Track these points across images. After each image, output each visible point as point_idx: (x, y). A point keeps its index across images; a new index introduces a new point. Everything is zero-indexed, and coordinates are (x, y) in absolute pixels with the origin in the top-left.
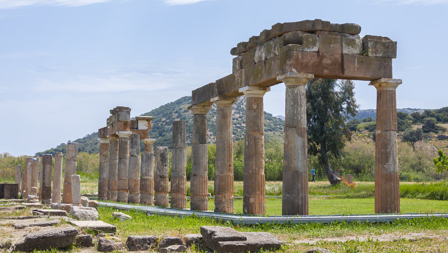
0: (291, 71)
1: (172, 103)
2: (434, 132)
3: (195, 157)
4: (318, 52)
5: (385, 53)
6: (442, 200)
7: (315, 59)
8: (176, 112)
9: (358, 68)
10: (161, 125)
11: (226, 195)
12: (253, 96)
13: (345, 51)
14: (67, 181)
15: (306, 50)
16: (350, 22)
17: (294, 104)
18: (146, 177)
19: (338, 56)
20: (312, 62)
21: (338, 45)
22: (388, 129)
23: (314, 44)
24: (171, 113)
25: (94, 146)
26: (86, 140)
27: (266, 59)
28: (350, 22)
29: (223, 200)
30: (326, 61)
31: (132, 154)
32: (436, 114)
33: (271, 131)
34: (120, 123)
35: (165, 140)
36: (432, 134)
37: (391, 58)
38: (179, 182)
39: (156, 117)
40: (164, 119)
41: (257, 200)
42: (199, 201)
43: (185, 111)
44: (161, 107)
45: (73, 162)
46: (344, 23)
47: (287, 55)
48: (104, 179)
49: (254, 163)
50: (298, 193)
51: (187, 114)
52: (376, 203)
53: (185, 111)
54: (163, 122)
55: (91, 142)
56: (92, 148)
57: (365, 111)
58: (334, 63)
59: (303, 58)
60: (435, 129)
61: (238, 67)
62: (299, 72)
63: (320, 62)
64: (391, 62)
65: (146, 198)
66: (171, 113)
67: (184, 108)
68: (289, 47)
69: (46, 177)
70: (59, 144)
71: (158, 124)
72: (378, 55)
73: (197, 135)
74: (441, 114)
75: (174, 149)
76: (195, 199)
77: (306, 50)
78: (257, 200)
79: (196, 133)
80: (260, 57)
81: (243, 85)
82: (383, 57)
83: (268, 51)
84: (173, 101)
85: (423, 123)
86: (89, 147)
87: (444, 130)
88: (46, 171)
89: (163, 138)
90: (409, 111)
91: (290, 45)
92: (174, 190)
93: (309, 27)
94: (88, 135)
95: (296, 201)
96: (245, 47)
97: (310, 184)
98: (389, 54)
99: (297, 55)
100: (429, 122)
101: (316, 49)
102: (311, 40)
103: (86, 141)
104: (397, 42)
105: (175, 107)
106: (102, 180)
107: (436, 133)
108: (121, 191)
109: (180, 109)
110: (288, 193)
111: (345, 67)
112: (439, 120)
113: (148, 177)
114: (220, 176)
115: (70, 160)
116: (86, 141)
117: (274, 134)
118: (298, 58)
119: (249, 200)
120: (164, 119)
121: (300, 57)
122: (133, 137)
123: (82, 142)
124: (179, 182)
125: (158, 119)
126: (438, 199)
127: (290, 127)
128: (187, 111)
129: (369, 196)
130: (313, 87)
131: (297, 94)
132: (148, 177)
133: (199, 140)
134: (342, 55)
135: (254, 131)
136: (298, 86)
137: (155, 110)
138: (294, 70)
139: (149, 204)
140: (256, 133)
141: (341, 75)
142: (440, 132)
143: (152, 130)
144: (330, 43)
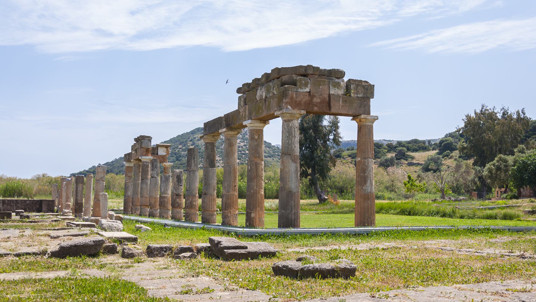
0: (287, 108)
2: (404, 159)
4: (310, 92)
5: (364, 94)
6: (410, 215)
7: (307, 98)
8: (191, 141)
9: (342, 106)
10: (178, 151)
12: (255, 128)
13: (332, 92)
16: (336, 68)
17: (289, 135)
19: (326, 96)
20: (304, 100)
21: (326, 87)
22: (366, 157)
23: (306, 85)
24: (186, 141)
26: (113, 163)
28: (336, 68)
29: (229, 215)
30: (316, 100)
32: (406, 145)
33: (270, 157)
35: (181, 164)
38: (192, 199)
39: (173, 144)
40: (180, 147)
41: (258, 215)
42: (209, 215)
43: (198, 140)
45: (102, 182)
47: (284, 95)
50: (292, 209)
54: (180, 148)
55: (118, 165)
57: (348, 141)
58: (322, 102)
59: (297, 97)
61: (242, 104)
62: (293, 108)
65: (164, 213)
66: (186, 141)
68: (285, 87)
72: (359, 96)
73: (208, 161)
74: (410, 145)
78: (258, 215)
79: (207, 158)
80: (261, 96)
82: (363, 98)
83: (268, 91)
85: (396, 152)
87: (413, 158)
88: (78, 189)
89: (180, 163)
90: (384, 142)
91: (286, 86)
93: (302, 71)
95: (290, 216)
98: (368, 95)
100: (400, 151)
101: (307, 90)
103: (114, 164)
105: (190, 136)
107: (407, 160)
108: (143, 207)
109: (195, 138)
110: (283, 210)
111: (332, 105)
112: (409, 149)
113: (166, 195)
115: (99, 180)
116: (114, 164)
119: (251, 215)
120: (180, 147)
121: (294, 96)
123: (111, 165)
124: (192, 199)
125: (176, 146)
126: (407, 215)
129: (350, 212)
131: (291, 127)
132: (166, 195)
133: (210, 165)
134: (329, 95)
135: (256, 157)
137: (173, 139)
139: (167, 218)
140: (257, 159)
141: (329, 112)
144: (319, 85)
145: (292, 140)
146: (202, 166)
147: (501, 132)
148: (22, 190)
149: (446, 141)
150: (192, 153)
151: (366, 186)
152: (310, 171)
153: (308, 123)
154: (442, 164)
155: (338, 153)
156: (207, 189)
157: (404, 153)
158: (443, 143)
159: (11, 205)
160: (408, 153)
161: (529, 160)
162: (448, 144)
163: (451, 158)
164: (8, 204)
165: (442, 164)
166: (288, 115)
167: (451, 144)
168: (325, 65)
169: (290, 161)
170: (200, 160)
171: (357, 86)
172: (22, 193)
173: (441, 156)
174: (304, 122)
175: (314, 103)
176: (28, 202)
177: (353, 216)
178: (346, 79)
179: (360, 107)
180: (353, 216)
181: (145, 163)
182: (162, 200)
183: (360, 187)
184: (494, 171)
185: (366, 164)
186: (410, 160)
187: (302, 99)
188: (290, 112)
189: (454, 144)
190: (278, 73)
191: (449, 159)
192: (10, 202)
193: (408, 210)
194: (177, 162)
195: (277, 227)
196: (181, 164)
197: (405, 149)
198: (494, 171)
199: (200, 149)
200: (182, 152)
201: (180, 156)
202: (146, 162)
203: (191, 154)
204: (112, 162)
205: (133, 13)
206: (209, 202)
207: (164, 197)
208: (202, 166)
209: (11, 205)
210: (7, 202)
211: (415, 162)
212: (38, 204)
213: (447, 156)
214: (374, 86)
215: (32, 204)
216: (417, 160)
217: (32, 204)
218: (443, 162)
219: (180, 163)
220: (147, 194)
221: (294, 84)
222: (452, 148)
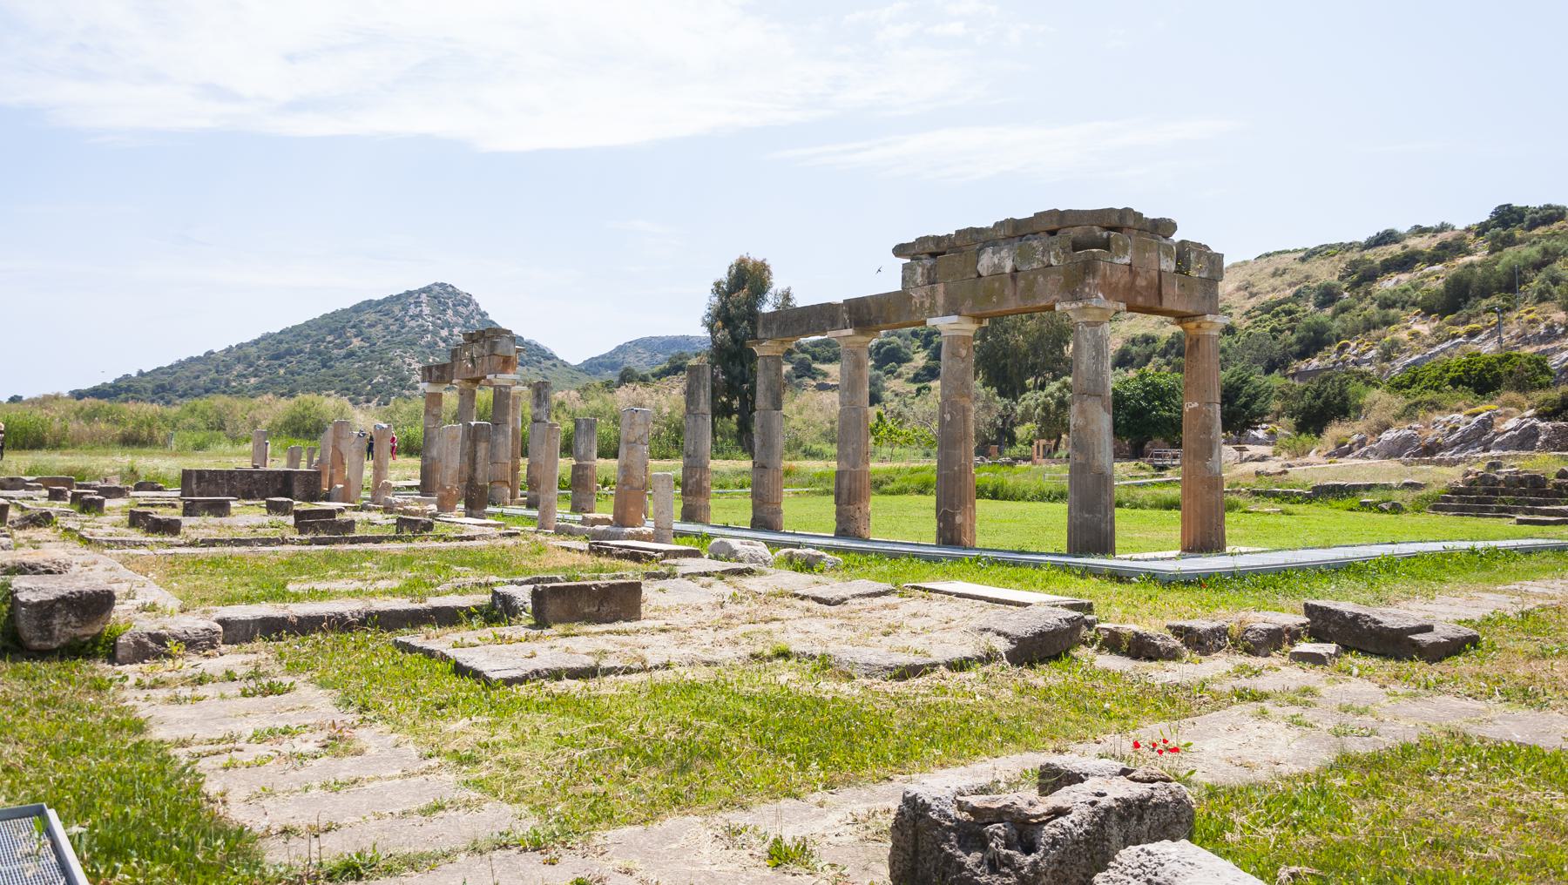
0: (1097, 297)
1: (344, 310)
2: (809, 377)
3: (764, 434)
4: (1130, 265)
5: (1211, 271)
6: (997, 499)
7: (1126, 278)
8: (354, 327)
9: (1178, 296)
10: (326, 347)
11: (862, 506)
12: (960, 333)
14: (628, 484)
15: (1116, 261)
16: (1167, 217)
17: (1098, 354)
18: (585, 462)
19: (1155, 274)
20: (1122, 282)
21: (1155, 254)
22: (1212, 400)
24: (344, 327)
25: (194, 381)
26: (175, 370)
27: (1015, 270)
28: (1167, 217)
29: (857, 515)
30: (1141, 282)
31: (538, 418)
32: (811, 349)
33: (523, 365)
34: (496, 358)
35: (335, 376)
36: (807, 380)
37: (1217, 281)
38: (701, 476)
39: (315, 333)
40: (329, 338)
41: (968, 519)
42: (772, 513)
43: (370, 326)
44: (324, 317)
45: (641, 447)
46: (1157, 217)
47: (1089, 268)
48: (432, 459)
49: (963, 453)
50: (1106, 511)
51: (373, 330)
52: (1183, 520)
53: (370, 326)
54: (329, 342)
55: (187, 374)
56: (190, 385)
57: (676, 337)
58: (1149, 286)
59: (1111, 274)
60: (813, 374)
62: (1107, 298)
63: (1133, 283)
64: (1217, 286)
65: (585, 500)
66: (344, 327)
67: (368, 319)
68: (1093, 253)
69: (478, 466)
70: (119, 376)
71: (319, 346)
72: (1202, 276)
73: (769, 394)
74: (817, 349)
75: (693, 417)
76: (765, 511)
77: (1116, 261)
78: (968, 519)
79: (767, 390)
81: (940, 313)
82: (1207, 279)
84: (348, 306)
85: (792, 363)
86: (182, 382)
87: (826, 375)
88: (479, 454)
89: (331, 372)
91: (1095, 250)
92: (691, 491)
93: (1115, 221)
94: (180, 361)
95: (1103, 525)
96: (937, 245)
97: (716, 465)
98: (1216, 274)
99: (1105, 268)
100: (802, 361)
101: (1127, 260)
102: (1121, 243)
103: (175, 373)
104: (1223, 255)
105: (352, 317)
106: (429, 461)
107: (814, 379)
108: (497, 485)
109: (362, 322)
110: (1089, 513)
111: (1163, 293)
112: (815, 358)
113: (589, 463)
114: (851, 472)
115: (635, 442)
116: (175, 373)
117: (528, 370)
118: (1106, 274)
119: (954, 519)
120: (329, 338)
121: (1108, 272)
122: (541, 385)
123: (168, 373)
124: (701, 476)
125: (320, 337)
126: (988, 498)
127: (1090, 395)
128: (374, 326)
129: (922, 490)
130: (733, 303)
131: (1102, 336)
132: (589, 463)
133: (773, 404)
134: (1160, 272)
135: (962, 396)
136: (1103, 323)
138: (1100, 295)
139: (505, 504)
140: (965, 399)
141: (1158, 307)
142: (820, 378)
143: (307, 356)
144: (1145, 251)
145: (1102, 366)
146: (381, 380)
147: (1037, 334)
148: (44, 432)
149: (889, 343)
150: (700, 375)
151: (1213, 461)
152: (736, 404)
153: (738, 308)
154: (884, 389)
155: (679, 362)
156: (767, 457)
157: (810, 365)
158: (883, 347)
159: (217, 484)
160: (813, 366)
161: (1125, 388)
162: (893, 349)
163: (899, 376)
164: (209, 482)
165: (884, 389)
166: (1097, 312)
167: (898, 349)
168: (1150, 213)
169: (1101, 409)
170: (377, 367)
171: (1200, 254)
172: (44, 438)
173: (881, 373)
174: (729, 305)
175: (1138, 289)
176: (256, 476)
177: (1062, 508)
178: (1176, 237)
179: (1204, 298)
180: (1062, 508)
181: (502, 389)
182: (580, 473)
183: (1199, 463)
184: (1053, 407)
185: (1212, 415)
186: (820, 379)
187: (1119, 279)
188: (1102, 306)
189: (903, 350)
190: (1053, 224)
191: (895, 378)
192: (216, 476)
193: (990, 488)
194: (323, 370)
195: (932, 540)
196: (335, 376)
197: (808, 356)
198: (1053, 407)
199: (375, 344)
200: (335, 351)
201: (331, 359)
202: (506, 387)
203: (698, 378)
204: (171, 367)
205: (291, 58)
206: (773, 484)
207: (586, 467)
208: (381, 380)
209: (217, 484)
210: (207, 476)
211: (831, 383)
212: (279, 479)
213: (892, 372)
214: (1223, 255)
215: (267, 479)
216: (833, 380)
217: (267, 479)
218: (885, 385)
219: (331, 372)
220: (506, 457)
221: (1106, 245)
222: (899, 358)
